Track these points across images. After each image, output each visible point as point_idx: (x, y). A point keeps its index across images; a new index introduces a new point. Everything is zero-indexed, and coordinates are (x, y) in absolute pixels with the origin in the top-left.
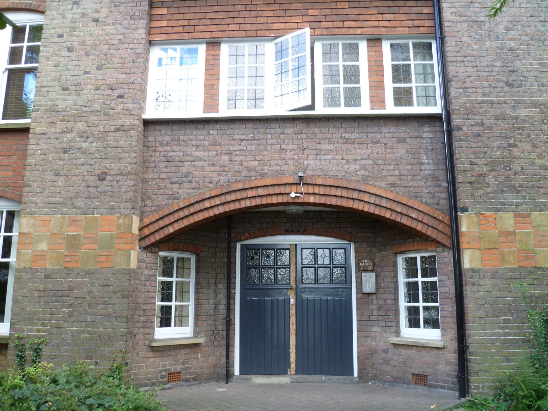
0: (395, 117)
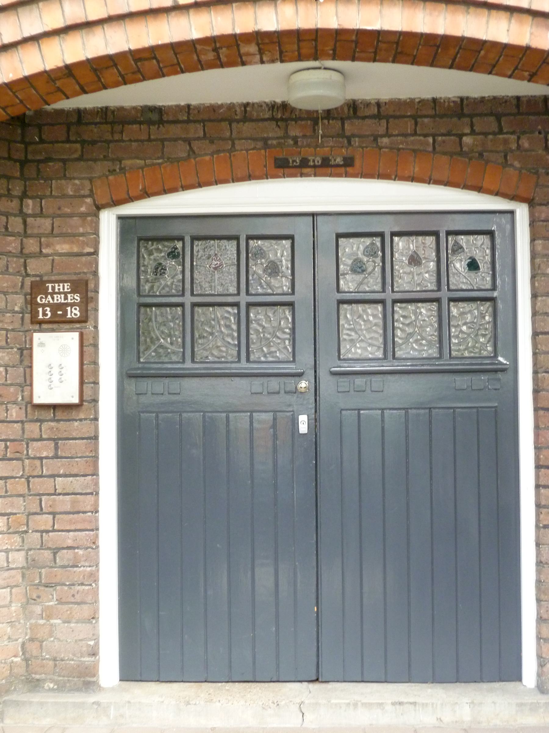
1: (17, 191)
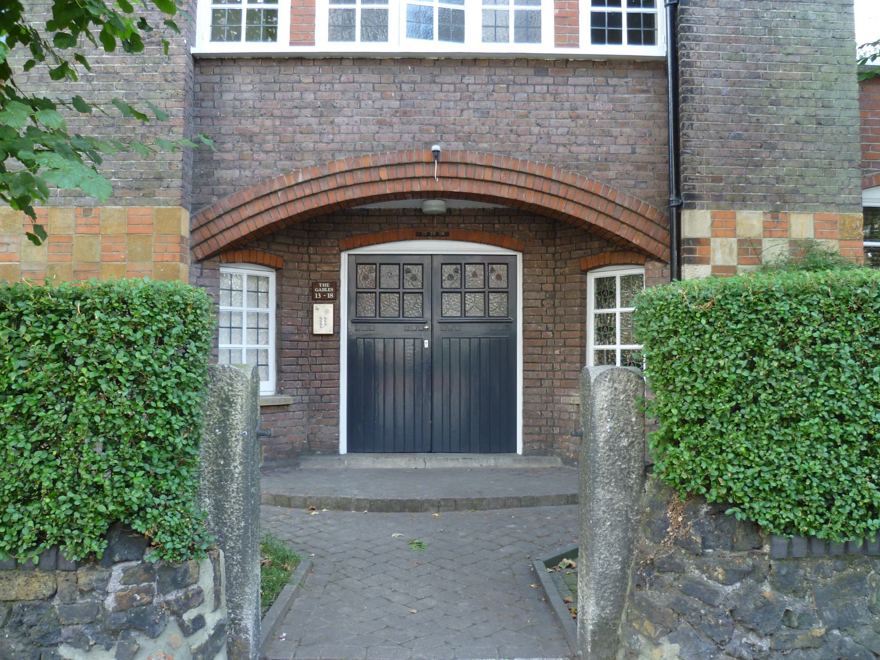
0: (325, 59)
1: (306, 244)
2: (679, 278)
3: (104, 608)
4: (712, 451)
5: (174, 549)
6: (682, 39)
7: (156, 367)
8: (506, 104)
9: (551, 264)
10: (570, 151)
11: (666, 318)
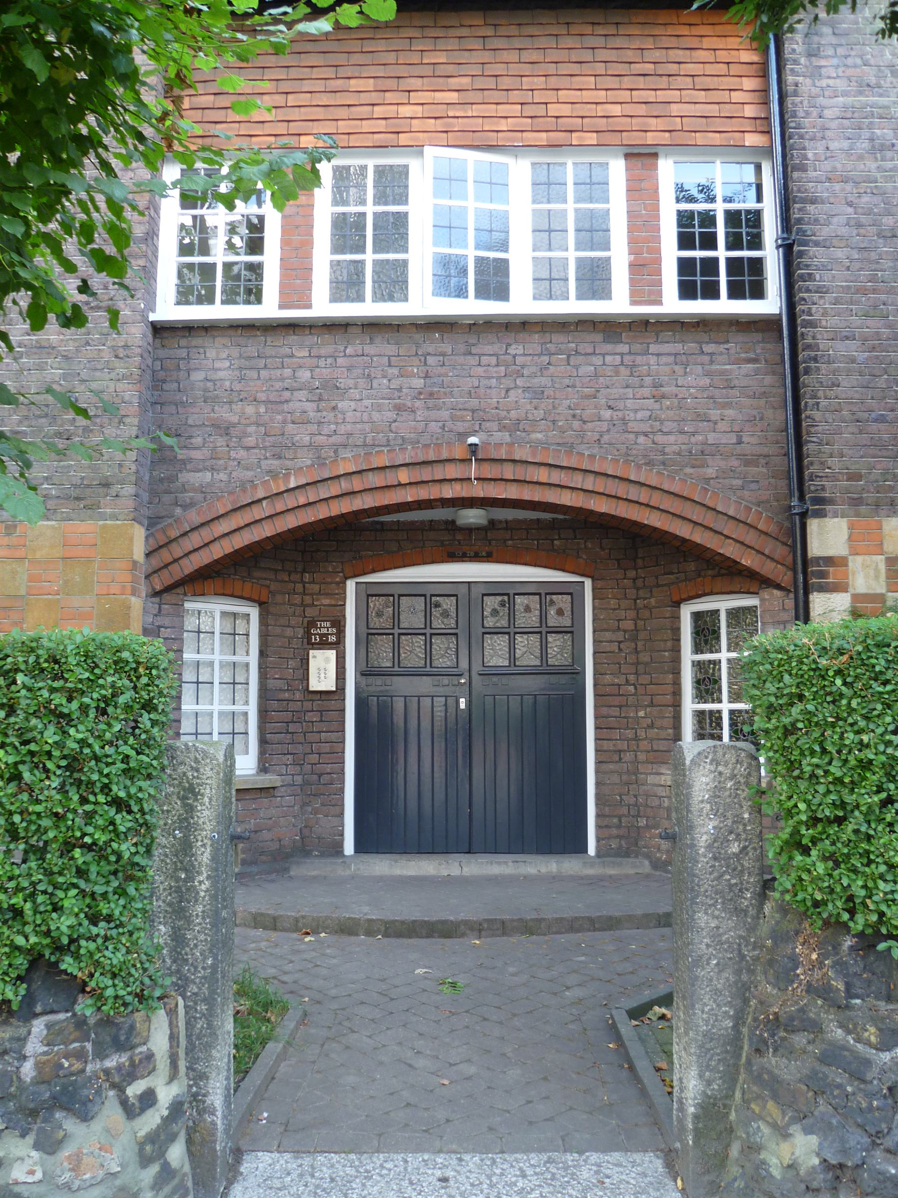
0: (325, 325)
1: (300, 569)
2: (807, 619)
3: (19, 1078)
4: (856, 862)
5: (116, 997)
6: (800, 290)
7: (97, 748)
8: (567, 381)
9: (632, 593)
10: (654, 443)
11: (786, 677)
